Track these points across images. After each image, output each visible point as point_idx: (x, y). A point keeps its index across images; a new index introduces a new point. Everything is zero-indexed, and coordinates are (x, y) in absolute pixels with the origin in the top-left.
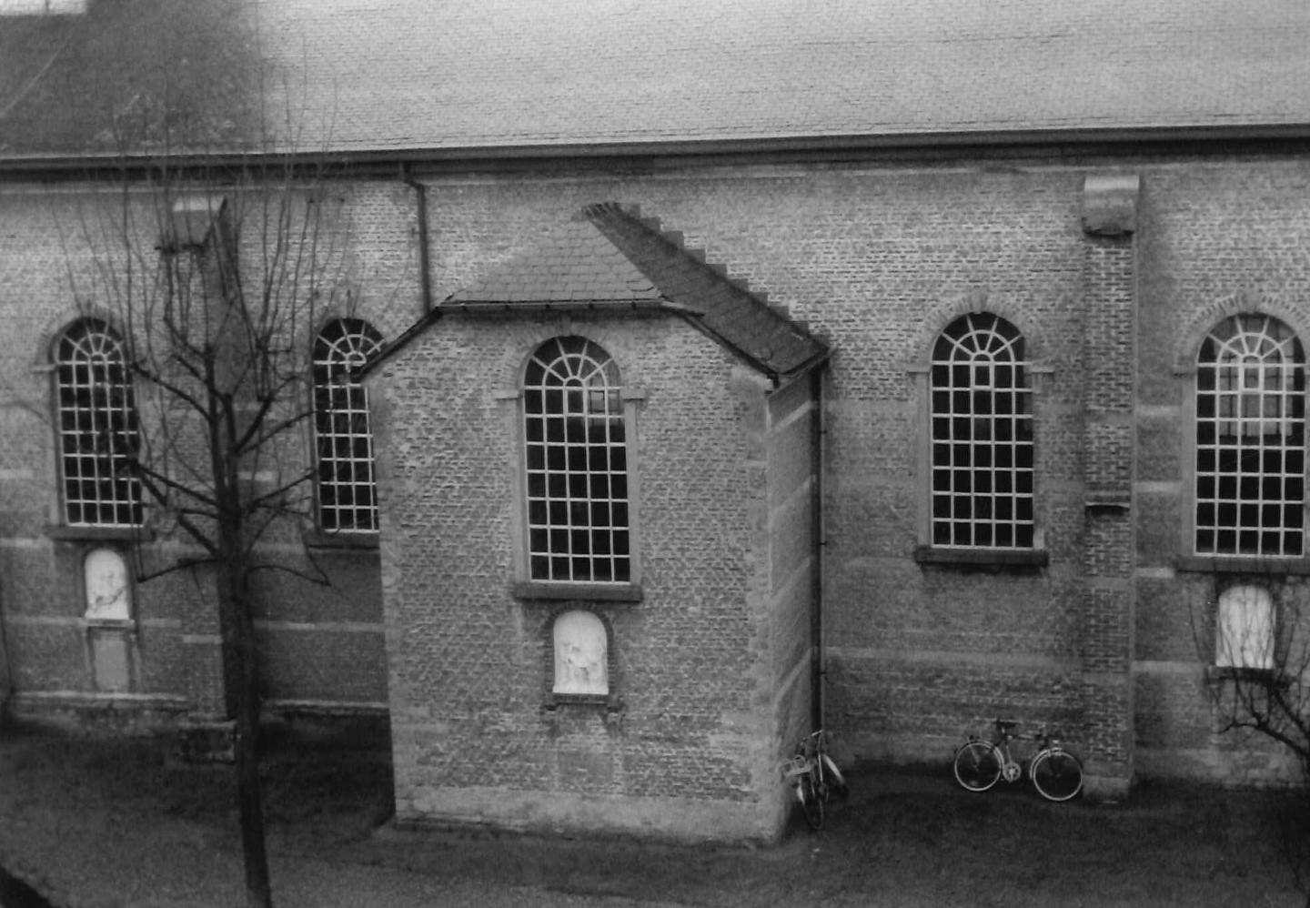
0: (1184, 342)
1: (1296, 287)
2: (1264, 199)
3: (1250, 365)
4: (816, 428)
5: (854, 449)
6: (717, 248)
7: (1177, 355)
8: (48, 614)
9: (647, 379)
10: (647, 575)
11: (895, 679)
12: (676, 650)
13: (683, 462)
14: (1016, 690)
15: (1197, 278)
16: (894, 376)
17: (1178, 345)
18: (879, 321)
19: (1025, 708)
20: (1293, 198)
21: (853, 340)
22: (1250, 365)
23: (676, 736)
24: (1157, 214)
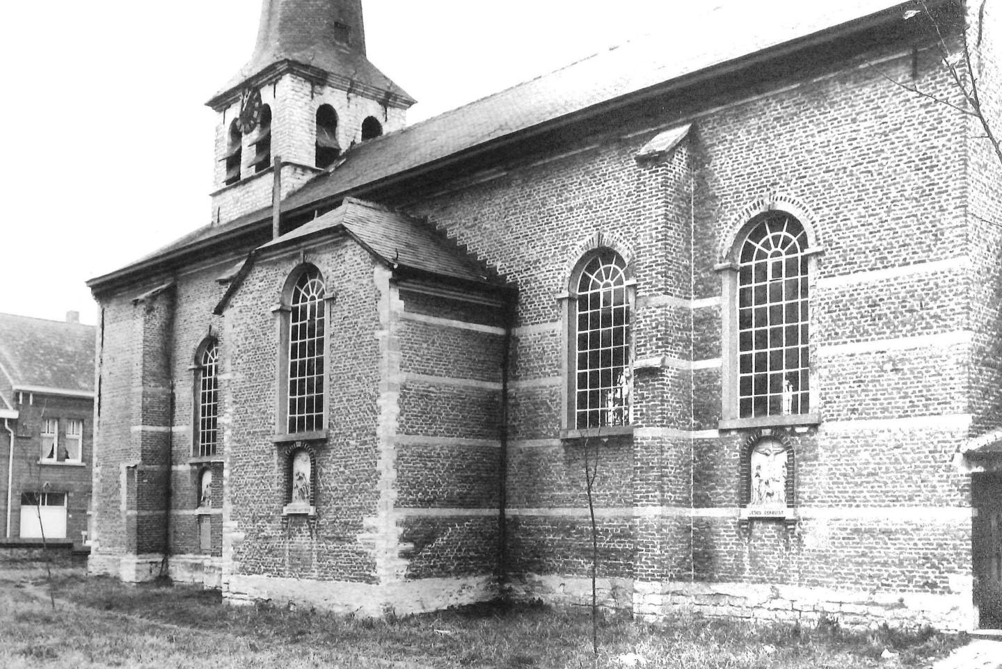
0: (723, 245)
1: (799, 184)
2: (775, 119)
3: (777, 259)
4: (224, 190)
5: (528, 361)
6: (463, 235)
7: (718, 256)
8: (187, 509)
9: (336, 284)
10: (332, 421)
11: (548, 531)
12: (343, 472)
13: (350, 338)
14: (620, 537)
15: (732, 192)
16: (551, 304)
17: (718, 249)
18: (543, 266)
19: (625, 551)
20: (795, 114)
21: (529, 283)
22: (777, 259)
23: (341, 536)
24: (706, 149)
